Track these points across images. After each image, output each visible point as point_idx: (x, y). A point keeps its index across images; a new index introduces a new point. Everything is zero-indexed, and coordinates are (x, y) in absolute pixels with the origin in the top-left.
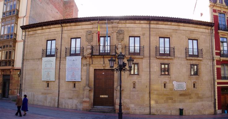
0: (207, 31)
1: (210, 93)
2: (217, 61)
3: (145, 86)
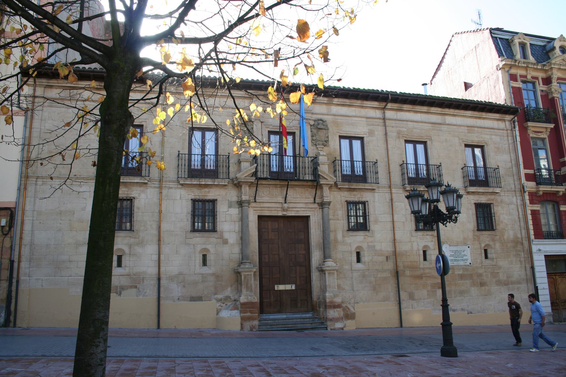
0: (501, 125)
1: (523, 272)
2: (531, 194)
3: (385, 258)
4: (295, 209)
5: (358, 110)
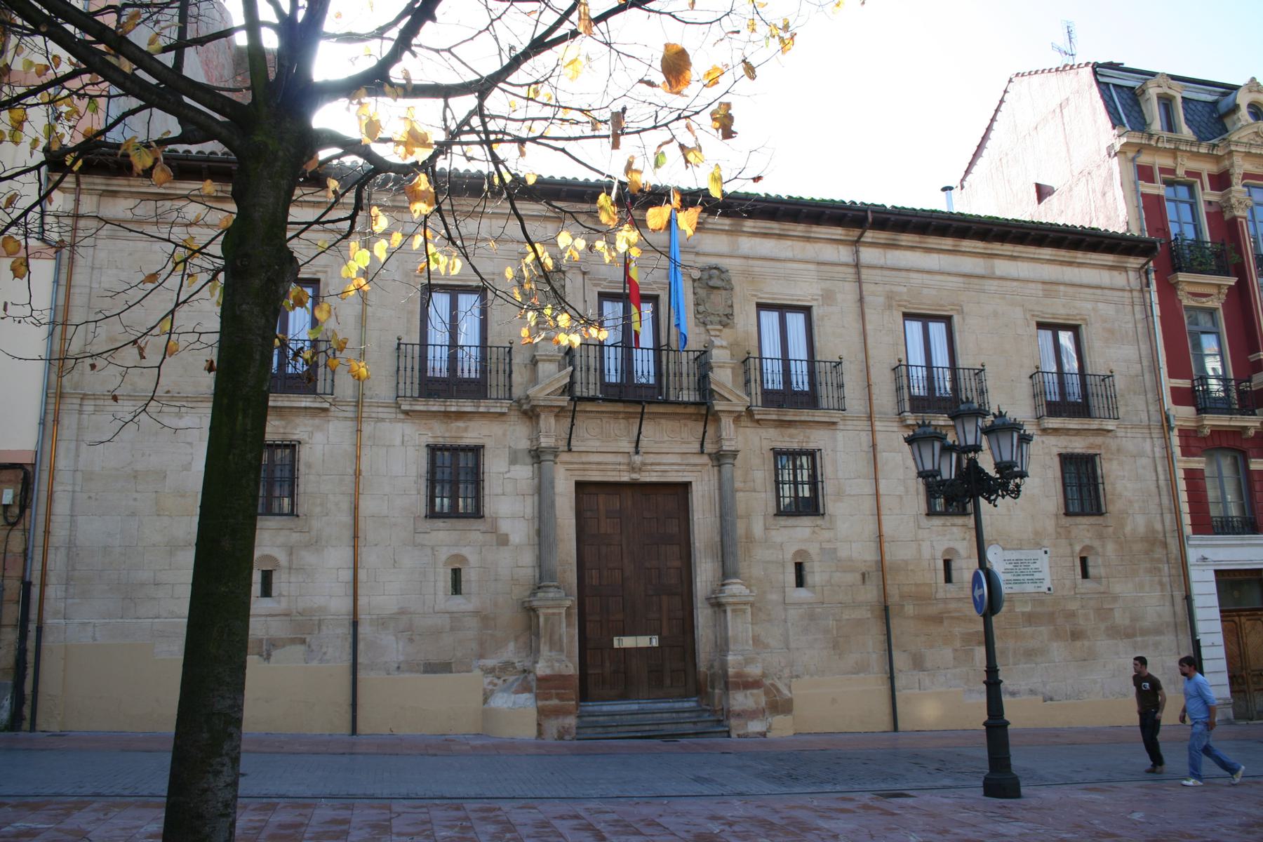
0: (1119, 279)
2: (1185, 434)
3: (858, 577)
4: (658, 468)
5: (799, 245)
